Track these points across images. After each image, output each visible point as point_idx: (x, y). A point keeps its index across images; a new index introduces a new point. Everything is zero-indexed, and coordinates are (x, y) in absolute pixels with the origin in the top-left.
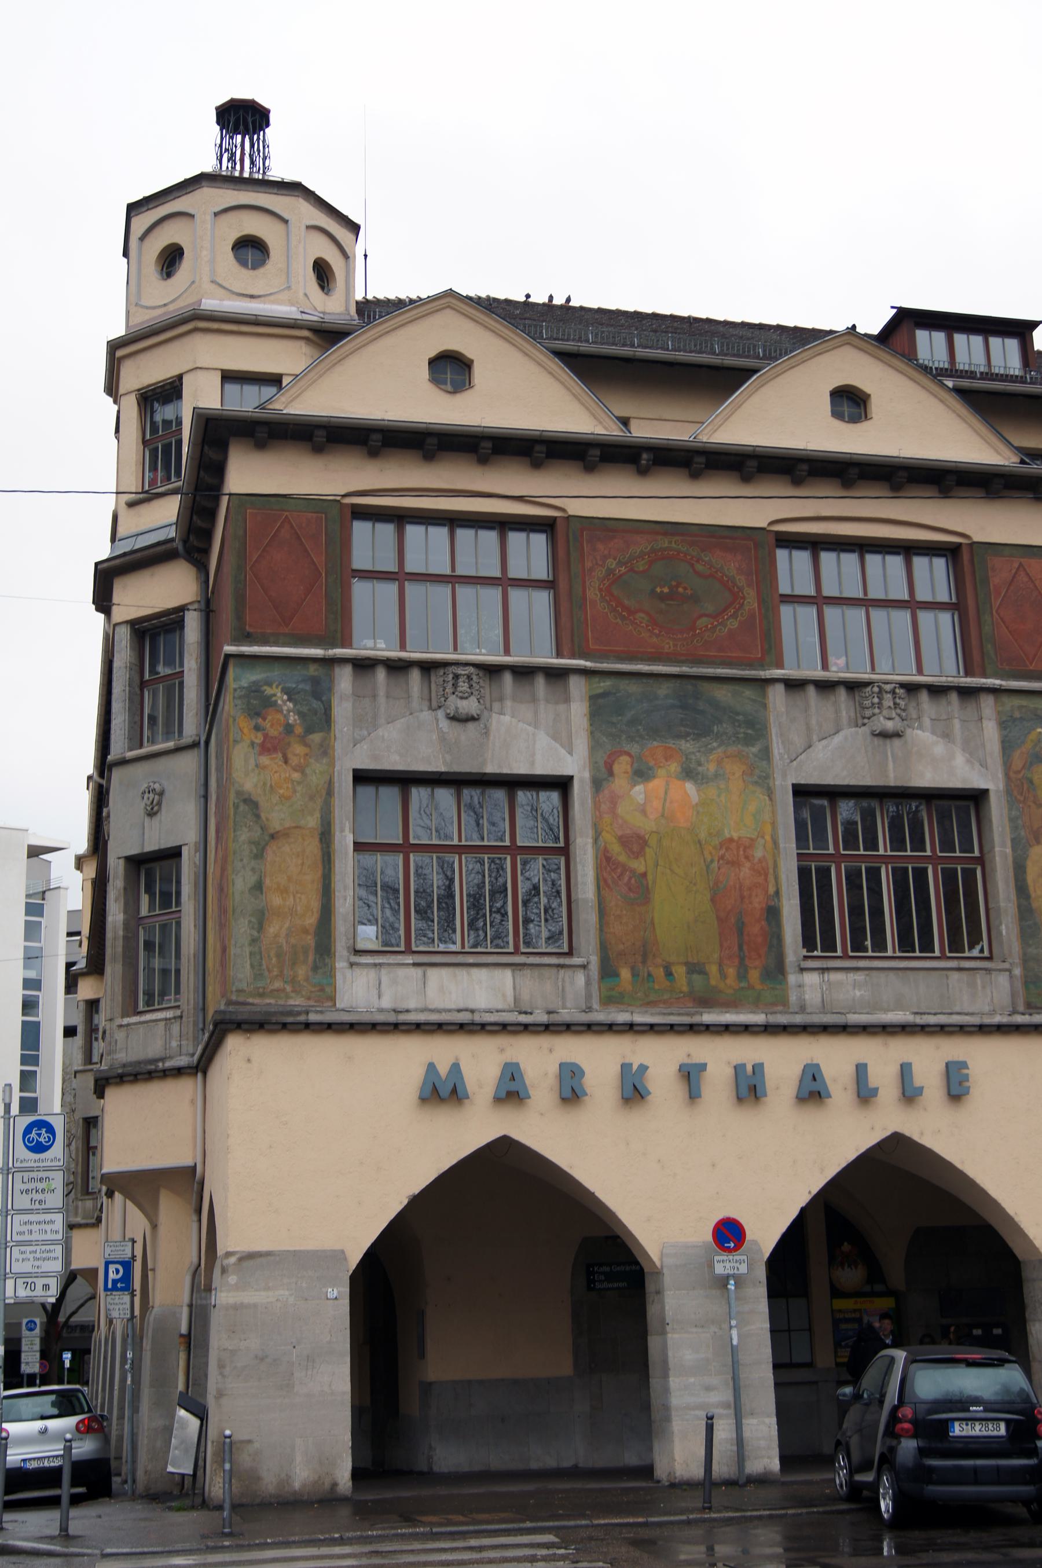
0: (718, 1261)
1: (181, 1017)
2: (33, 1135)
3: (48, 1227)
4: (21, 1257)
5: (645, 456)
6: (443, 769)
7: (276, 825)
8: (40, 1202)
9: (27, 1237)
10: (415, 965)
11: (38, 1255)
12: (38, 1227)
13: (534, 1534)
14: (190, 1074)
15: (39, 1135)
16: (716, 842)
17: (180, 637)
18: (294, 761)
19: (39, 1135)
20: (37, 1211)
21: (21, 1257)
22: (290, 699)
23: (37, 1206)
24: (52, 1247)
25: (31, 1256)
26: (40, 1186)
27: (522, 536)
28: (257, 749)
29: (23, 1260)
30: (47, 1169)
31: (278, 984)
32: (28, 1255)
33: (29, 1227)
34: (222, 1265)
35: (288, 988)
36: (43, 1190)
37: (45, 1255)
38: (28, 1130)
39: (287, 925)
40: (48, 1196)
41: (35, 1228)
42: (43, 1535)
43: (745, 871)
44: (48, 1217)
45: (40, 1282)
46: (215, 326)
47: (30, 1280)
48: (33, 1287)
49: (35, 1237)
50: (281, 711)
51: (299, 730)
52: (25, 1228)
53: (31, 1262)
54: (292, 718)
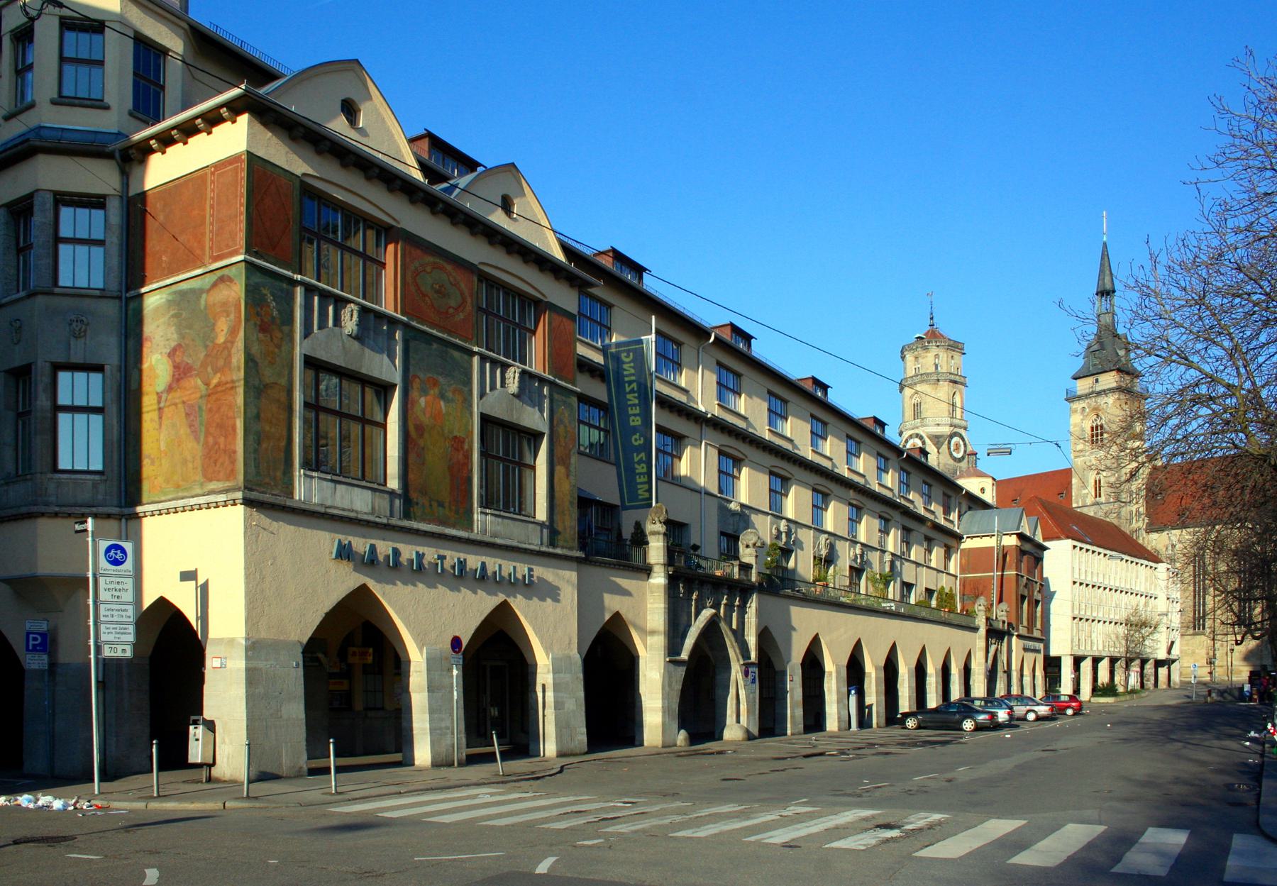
0: (129, 617)
1: (106, 481)
2: (112, 553)
3: (124, 614)
4: (107, 631)
5: (441, 206)
6: (343, 365)
7: (267, 381)
8: (118, 597)
9: (110, 619)
10: (332, 481)
11: (118, 631)
12: (117, 613)
13: (469, 806)
14: (116, 519)
15: (116, 554)
16: (451, 436)
17: (25, 226)
18: (276, 341)
19: (116, 554)
20: (117, 603)
21: (107, 631)
22: (274, 300)
23: (116, 600)
24: (127, 626)
25: (113, 631)
26: (118, 587)
27: (71, 210)
28: (258, 328)
29: (108, 633)
30: (120, 576)
31: (267, 480)
32: (111, 630)
33: (112, 613)
34: (916, 729)
35: (272, 484)
36: (120, 590)
37: (122, 631)
38: (108, 550)
39: (272, 444)
40: (122, 594)
41: (115, 613)
42: (320, 825)
43: (461, 456)
44: (123, 607)
45: (120, 648)
46: (168, 16)
47: (113, 646)
48: (116, 651)
49: (115, 619)
50: (269, 306)
51: (278, 321)
52: (108, 613)
53: (114, 635)
54: (275, 313)
